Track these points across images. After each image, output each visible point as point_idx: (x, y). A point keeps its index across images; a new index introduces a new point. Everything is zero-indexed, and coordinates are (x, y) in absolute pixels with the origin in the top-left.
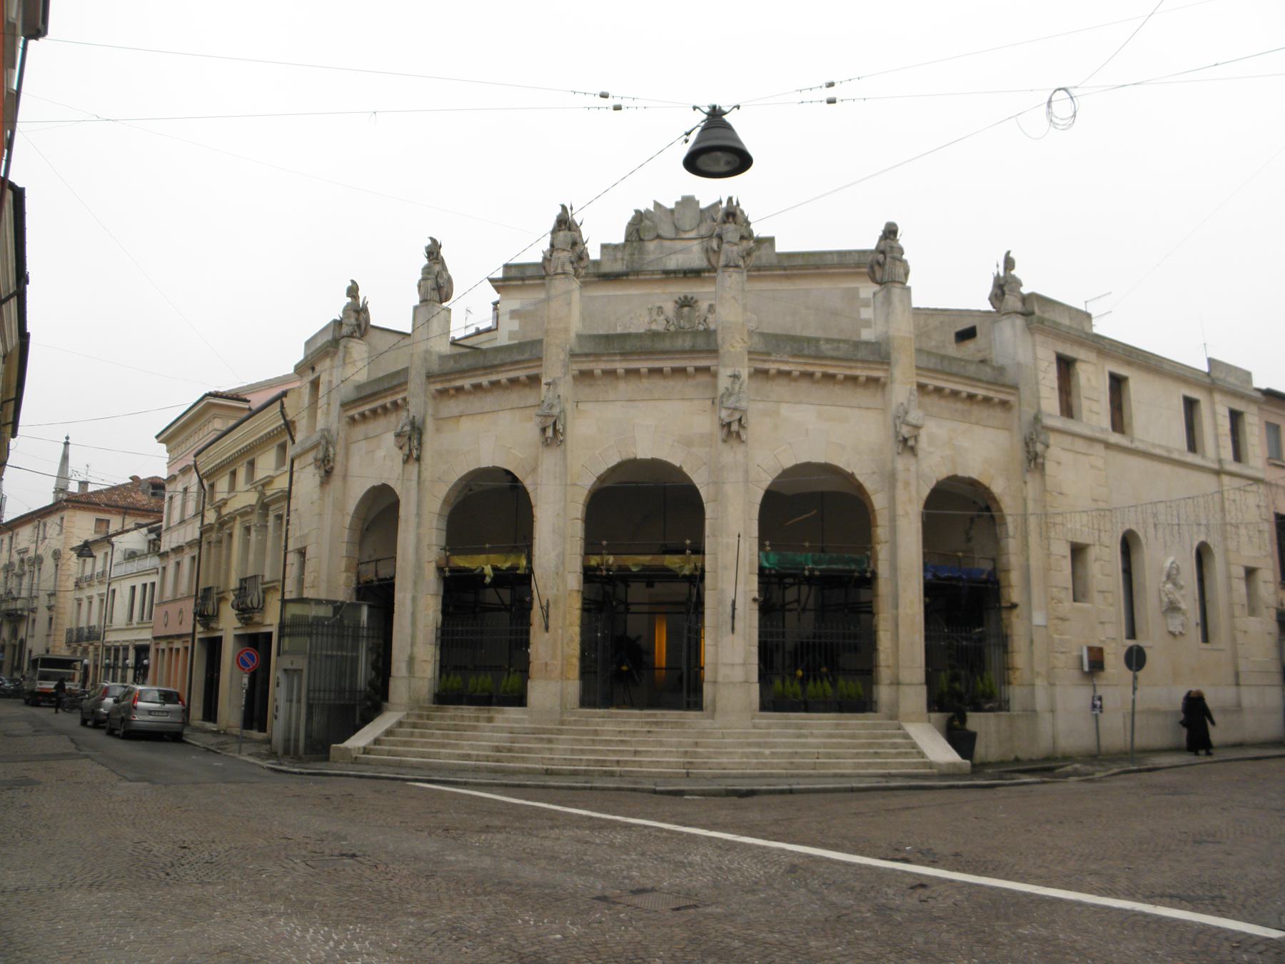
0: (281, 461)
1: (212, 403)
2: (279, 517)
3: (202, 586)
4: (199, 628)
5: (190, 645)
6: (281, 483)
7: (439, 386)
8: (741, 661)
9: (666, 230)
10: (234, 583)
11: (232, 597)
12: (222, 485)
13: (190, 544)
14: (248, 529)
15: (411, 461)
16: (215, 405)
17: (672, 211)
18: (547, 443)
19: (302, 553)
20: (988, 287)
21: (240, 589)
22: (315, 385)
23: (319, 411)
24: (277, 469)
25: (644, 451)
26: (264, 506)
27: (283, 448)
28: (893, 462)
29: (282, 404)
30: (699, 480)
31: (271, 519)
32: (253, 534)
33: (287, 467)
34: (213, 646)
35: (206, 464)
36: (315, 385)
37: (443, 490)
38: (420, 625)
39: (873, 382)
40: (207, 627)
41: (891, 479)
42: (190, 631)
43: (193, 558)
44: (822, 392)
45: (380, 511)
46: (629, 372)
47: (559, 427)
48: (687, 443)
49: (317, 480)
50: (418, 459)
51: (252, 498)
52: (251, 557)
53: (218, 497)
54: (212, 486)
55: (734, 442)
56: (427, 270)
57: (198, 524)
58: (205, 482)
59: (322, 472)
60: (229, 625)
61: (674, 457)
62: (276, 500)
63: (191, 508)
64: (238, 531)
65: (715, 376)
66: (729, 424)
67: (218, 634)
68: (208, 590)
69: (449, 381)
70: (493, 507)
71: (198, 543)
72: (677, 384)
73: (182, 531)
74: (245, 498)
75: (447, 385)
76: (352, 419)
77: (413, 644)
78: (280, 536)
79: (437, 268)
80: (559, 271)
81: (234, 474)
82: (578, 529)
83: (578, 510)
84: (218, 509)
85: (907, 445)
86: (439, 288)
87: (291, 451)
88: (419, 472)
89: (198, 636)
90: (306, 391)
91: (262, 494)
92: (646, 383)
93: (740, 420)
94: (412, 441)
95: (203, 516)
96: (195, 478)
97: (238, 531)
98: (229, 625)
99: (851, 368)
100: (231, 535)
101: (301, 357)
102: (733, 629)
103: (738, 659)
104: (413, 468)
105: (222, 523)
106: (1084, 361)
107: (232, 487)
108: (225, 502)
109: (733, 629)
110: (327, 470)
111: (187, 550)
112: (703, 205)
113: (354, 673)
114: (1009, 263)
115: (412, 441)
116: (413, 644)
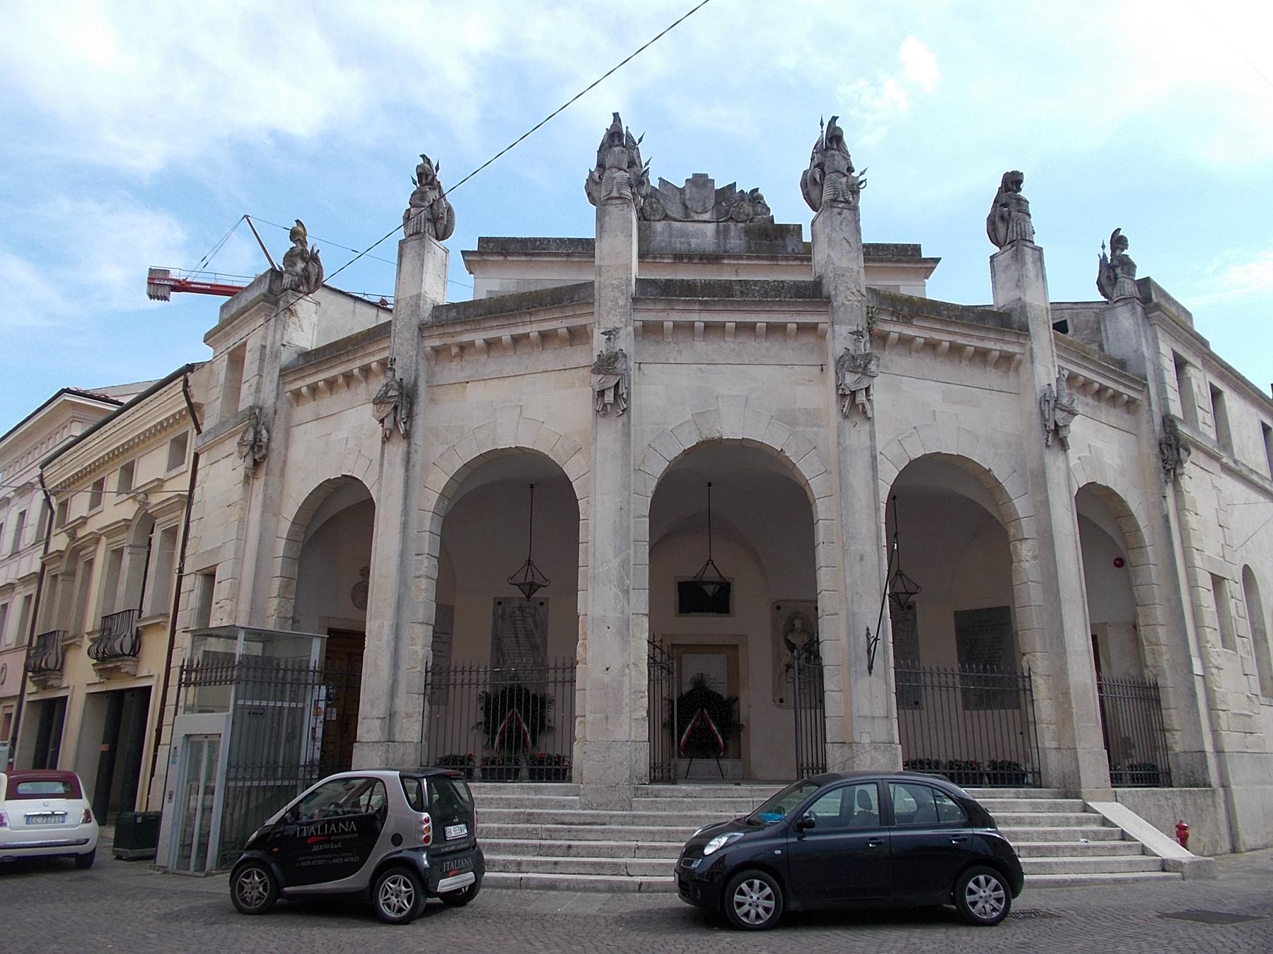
0: (176, 458)
1: (67, 402)
2: (171, 533)
3: (39, 631)
4: (31, 687)
5: (14, 711)
6: (181, 485)
7: (437, 342)
8: (884, 713)
9: (675, 210)
10: (91, 622)
11: (87, 643)
12: (79, 505)
13: (24, 580)
14: (118, 553)
15: (395, 440)
16: (74, 404)
17: (682, 191)
18: (603, 411)
19: (209, 576)
20: (1093, 271)
21: (103, 630)
22: (236, 359)
23: (244, 387)
24: (169, 469)
25: (731, 429)
26: (146, 522)
27: (180, 444)
28: (1042, 457)
29: (186, 381)
30: (809, 469)
31: (157, 537)
32: (126, 558)
33: (188, 465)
34: (52, 712)
35: (55, 476)
36: (236, 359)
37: (439, 480)
38: (404, 666)
39: (1006, 360)
40: (43, 685)
41: (1039, 480)
42: (18, 693)
43: (28, 598)
44: (945, 368)
45: (339, 517)
46: (708, 327)
47: (622, 390)
48: (788, 419)
49: (241, 471)
50: (407, 436)
51: (128, 510)
52: (122, 588)
53: (73, 515)
54: (64, 505)
55: (856, 418)
56: (417, 199)
57: (41, 553)
58: (53, 500)
59: (249, 462)
60: (80, 677)
61: (774, 438)
62: (167, 507)
63: (30, 534)
64: (101, 556)
65: (822, 337)
66: (854, 393)
67: (61, 694)
68: (47, 639)
69: (453, 335)
70: (515, 504)
71: (40, 576)
72: (772, 347)
73: (14, 566)
74: (117, 509)
75: (448, 340)
76: (297, 395)
77: (393, 693)
78: (172, 555)
79: (432, 195)
80: (615, 194)
81: (99, 485)
82: (643, 528)
83: (643, 506)
84: (72, 535)
85: (1057, 436)
86: (434, 220)
87: (192, 445)
88: (408, 453)
89: (27, 698)
90: (222, 365)
91: (144, 504)
92: (730, 344)
93: (867, 389)
94: (400, 408)
95: (47, 544)
96: (39, 496)
97: (101, 556)
98: (80, 677)
99: (982, 339)
100: (90, 563)
101: (217, 323)
102: (870, 668)
103: (880, 711)
104: (397, 450)
105: (74, 552)
106: (1193, 366)
107: (96, 501)
108: (84, 521)
109: (870, 668)
110: (258, 456)
111: (19, 589)
112: (718, 186)
113: (294, 736)
114: (1118, 241)
115: (400, 408)
116: (393, 693)
